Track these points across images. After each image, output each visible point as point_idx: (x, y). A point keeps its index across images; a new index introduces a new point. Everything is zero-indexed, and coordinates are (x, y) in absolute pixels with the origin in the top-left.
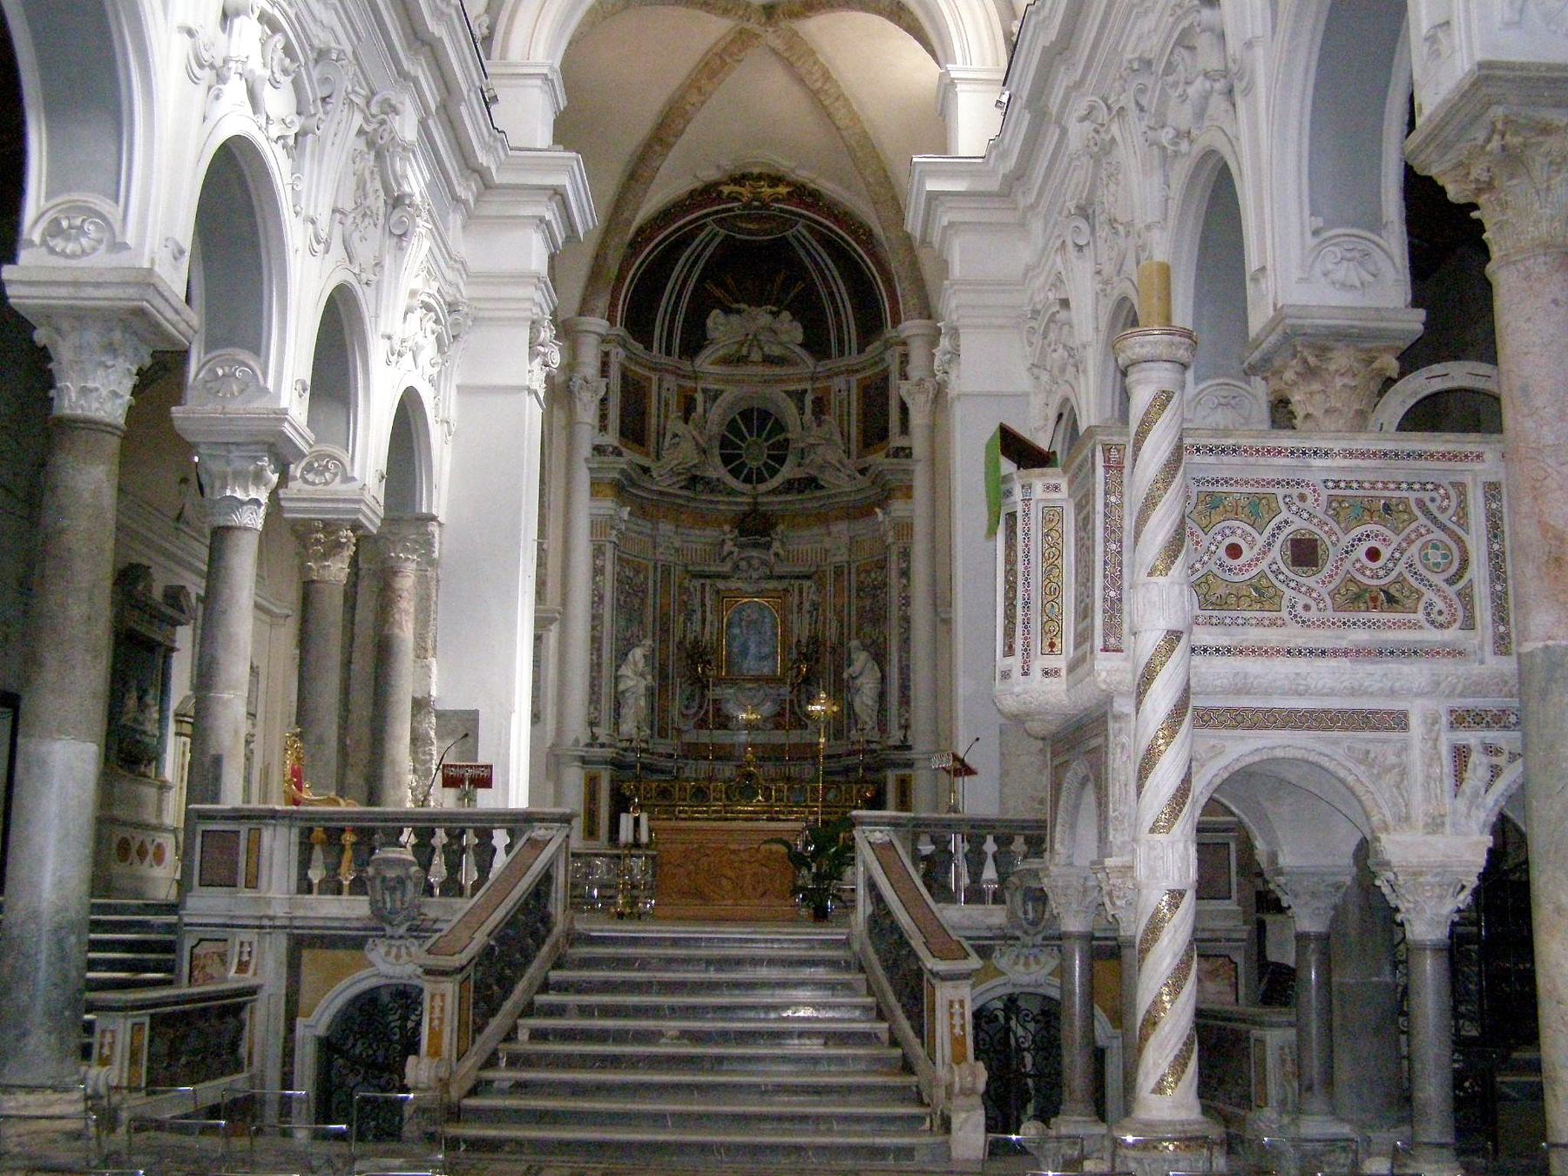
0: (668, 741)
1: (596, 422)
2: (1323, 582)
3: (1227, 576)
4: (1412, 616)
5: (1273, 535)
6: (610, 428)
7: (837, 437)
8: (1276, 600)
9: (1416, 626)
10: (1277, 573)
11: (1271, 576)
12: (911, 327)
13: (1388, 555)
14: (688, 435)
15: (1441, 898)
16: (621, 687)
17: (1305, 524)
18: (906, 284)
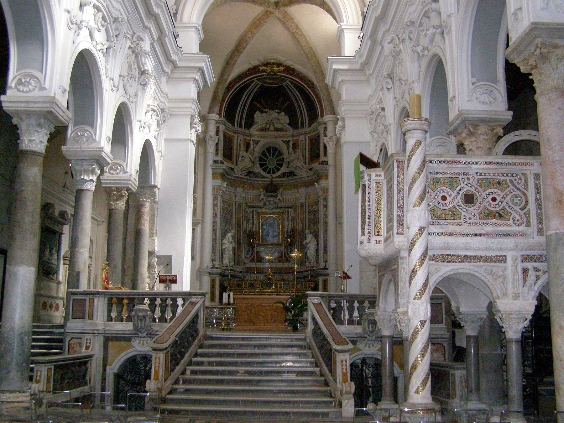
0: (240, 267)
1: (214, 152)
2: (476, 209)
3: (441, 207)
4: (508, 222)
5: (458, 193)
6: (219, 154)
7: (301, 157)
8: (459, 216)
9: (509, 225)
10: (459, 206)
11: (457, 207)
12: (328, 118)
13: (499, 200)
14: (247, 157)
15: (518, 323)
16: (224, 247)
17: (469, 189)
18: (326, 102)
